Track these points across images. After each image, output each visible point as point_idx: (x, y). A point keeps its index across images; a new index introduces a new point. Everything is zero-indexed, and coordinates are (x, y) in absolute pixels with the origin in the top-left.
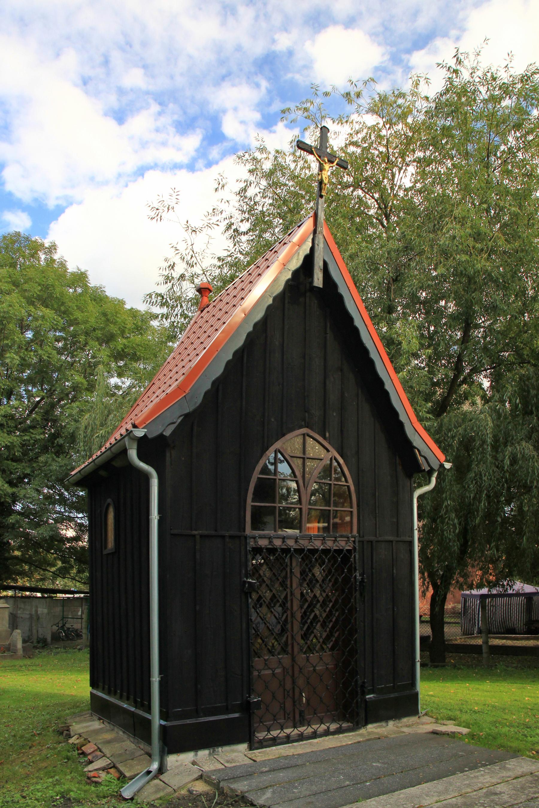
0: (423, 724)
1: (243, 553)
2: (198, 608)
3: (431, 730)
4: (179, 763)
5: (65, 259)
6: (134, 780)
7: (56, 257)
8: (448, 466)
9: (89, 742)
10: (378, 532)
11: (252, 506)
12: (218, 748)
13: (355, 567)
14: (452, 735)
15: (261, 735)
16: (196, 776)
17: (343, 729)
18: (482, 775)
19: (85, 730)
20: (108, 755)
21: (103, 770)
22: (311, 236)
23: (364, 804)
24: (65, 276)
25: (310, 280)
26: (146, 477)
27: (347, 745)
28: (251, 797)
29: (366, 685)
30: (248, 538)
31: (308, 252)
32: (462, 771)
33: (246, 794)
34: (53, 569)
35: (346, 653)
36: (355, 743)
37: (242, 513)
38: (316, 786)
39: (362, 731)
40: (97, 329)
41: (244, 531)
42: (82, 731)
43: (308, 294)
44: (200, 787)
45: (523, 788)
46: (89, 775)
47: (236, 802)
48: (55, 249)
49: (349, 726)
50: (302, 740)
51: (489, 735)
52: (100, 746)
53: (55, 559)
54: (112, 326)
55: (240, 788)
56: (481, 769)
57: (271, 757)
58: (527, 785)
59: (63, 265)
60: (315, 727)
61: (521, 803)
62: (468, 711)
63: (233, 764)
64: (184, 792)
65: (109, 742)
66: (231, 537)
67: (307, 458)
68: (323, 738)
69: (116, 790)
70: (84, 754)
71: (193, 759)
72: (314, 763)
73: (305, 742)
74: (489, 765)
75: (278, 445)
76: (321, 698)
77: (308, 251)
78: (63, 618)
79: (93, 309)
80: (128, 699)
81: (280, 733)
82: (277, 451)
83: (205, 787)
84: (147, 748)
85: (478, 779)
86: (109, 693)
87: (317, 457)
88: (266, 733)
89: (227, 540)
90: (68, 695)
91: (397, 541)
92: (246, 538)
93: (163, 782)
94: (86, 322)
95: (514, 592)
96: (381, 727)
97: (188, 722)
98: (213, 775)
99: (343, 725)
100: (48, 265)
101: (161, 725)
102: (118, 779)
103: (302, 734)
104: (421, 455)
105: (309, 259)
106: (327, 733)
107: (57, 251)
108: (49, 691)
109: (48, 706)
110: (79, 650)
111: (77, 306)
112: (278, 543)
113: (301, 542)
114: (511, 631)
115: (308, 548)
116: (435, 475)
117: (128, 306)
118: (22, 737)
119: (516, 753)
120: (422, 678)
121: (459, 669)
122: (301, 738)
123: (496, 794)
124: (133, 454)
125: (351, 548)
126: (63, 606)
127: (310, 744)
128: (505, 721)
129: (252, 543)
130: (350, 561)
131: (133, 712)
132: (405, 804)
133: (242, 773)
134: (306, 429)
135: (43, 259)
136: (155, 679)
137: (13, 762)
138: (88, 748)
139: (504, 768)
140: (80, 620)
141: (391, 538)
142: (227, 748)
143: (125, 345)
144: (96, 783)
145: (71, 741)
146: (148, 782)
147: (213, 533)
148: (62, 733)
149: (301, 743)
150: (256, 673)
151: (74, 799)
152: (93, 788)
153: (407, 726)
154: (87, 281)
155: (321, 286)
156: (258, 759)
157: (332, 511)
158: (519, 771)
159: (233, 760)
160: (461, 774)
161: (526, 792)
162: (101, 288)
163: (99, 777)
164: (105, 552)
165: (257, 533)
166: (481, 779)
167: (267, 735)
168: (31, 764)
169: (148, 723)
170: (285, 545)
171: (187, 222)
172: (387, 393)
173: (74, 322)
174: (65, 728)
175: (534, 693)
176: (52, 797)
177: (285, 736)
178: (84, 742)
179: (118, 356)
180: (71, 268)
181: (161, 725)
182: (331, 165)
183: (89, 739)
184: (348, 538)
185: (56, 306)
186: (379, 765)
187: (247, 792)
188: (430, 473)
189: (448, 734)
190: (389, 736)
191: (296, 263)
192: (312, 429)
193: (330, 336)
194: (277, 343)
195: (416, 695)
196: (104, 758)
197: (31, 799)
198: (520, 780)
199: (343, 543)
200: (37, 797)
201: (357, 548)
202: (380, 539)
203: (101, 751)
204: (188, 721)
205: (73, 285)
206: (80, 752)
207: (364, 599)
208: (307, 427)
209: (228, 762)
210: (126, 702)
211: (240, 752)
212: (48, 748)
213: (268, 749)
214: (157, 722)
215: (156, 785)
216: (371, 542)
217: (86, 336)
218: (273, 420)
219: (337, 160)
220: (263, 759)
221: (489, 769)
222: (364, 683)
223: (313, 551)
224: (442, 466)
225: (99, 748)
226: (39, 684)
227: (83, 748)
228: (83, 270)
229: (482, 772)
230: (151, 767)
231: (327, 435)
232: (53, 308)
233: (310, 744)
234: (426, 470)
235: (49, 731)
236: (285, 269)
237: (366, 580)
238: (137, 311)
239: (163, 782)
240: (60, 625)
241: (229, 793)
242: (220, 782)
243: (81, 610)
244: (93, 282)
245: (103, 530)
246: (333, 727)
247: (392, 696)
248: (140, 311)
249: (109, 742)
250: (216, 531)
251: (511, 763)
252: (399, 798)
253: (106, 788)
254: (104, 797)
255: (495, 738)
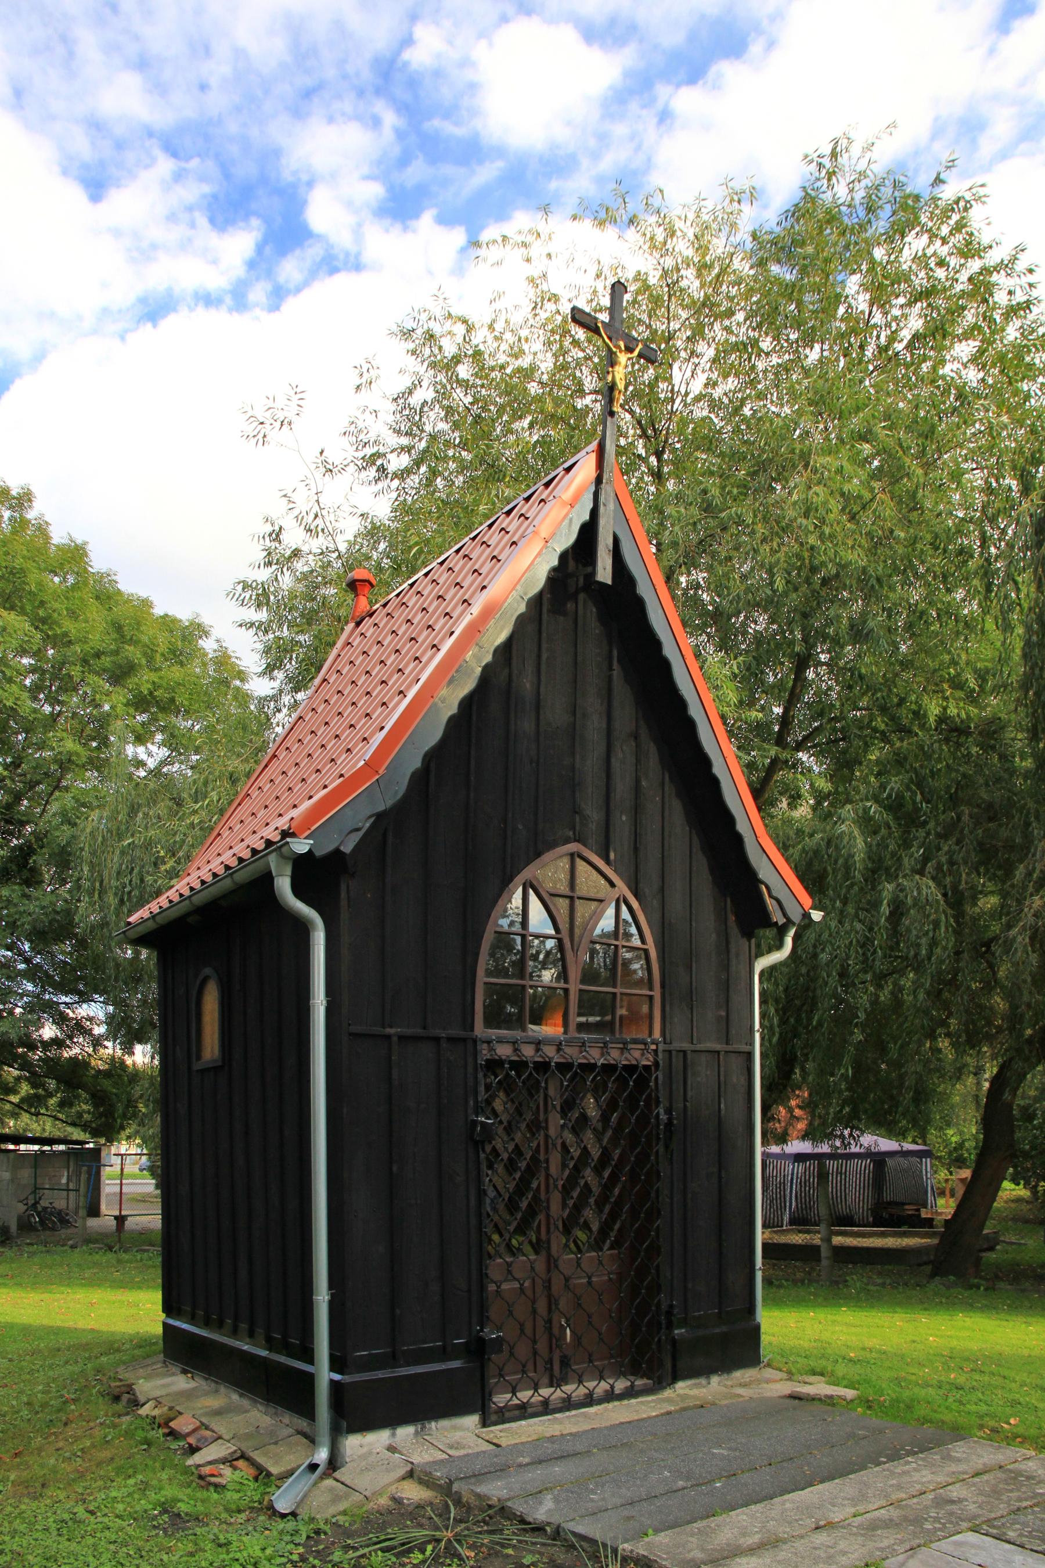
0: (768, 1381)
1: (470, 1069)
2: (395, 1168)
3: (788, 1392)
4: (365, 1450)
5: (46, 519)
6: (291, 1479)
7: (31, 515)
8: (817, 916)
9: (180, 1413)
10: (695, 1034)
11: (485, 983)
12: (430, 1423)
13: (658, 1098)
14: (829, 1401)
15: (501, 1399)
16: (402, 1471)
17: (636, 1388)
18: (915, 1470)
19: (163, 1392)
20: (227, 1437)
21: (224, 1463)
22: (593, 488)
23: (728, 1520)
24: (47, 549)
25: (589, 569)
26: (303, 928)
27: (649, 1418)
28: (519, 1507)
29: (676, 1311)
30: (479, 1043)
31: (588, 518)
32: (878, 1464)
33: (509, 1504)
34: (15, 1099)
35: (642, 1254)
36: (662, 1414)
37: (469, 997)
38: (628, 1489)
39: (668, 1393)
40: (103, 653)
41: (472, 1029)
42: (157, 1393)
43: (582, 596)
44: (413, 1493)
45: (996, 1493)
46: (203, 1473)
47: (491, 1517)
48: (30, 501)
49: (645, 1384)
50: (568, 1410)
51: (898, 1401)
52: (204, 1420)
53: (18, 1079)
54: (131, 648)
55: (494, 1492)
56: (909, 1459)
57: (524, 1439)
58: (1001, 1486)
59: (42, 530)
60: (591, 1384)
61: (1002, 1517)
62: (840, 1360)
63: (462, 1452)
64: (384, 1501)
65: (218, 1413)
66: (451, 1040)
67: (579, 898)
68: (603, 1406)
69: (256, 1498)
70: (173, 1434)
71: (387, 1442)
72: (605, 1448)
73: (574, 1412)
74: (922, 1452)
75: (526, 874)
76: (600, 1334)
77: (586, 517)
78: (36, 1188)
79: (96, 615)
80: (251, 1334)
81: (533, 1396)
82: (528, 885)
83: (422, 1492)
84: (303, 1424)
85: (911, 1476)
86: (207, 1324)
87: (592, 895)
88: (510, 1395)
89: (444, 1044)
90: (84, 1330)
91: (726, 1052)
92: (475, 1041)
93: (343, 1483)
94: (85, 641)
95: (862, 1150)
96: (696, 1386)
97: (381, 1376)
98: (436, 1470)
99: (637, 1383)
100: (15, 532)
101: (332, 1381)
102: (256, 1479)
103: (569, 1397)
104: (771, 896)
105: (588, 532)
106: (610, 1396)
107: (34, 504)
108: (46, 1322)
109: (59, 1350)
110: (72, 1247)
111: (67, 609)
112: (528, 1051)
113: (568, 1050)
114: (844, 1221)
115: (580, 1061)
116: (792, 932)
117: (158, 611)
118: (44, 1405)
119: (957, 1433)
120: (767, 1301)
121: (780, 1286)
122: (568, 1404)
123: (953, 1502)
124: (284, 885)
125: (649, 1063)
126: (36, 1167)
127: (585, 1415)
128: (913, 1378)
129: (485, 1053)
130: (649, 1086)
131: (265, 1358)
132: (801, 1519)
133: (486, 1466)
134: (576, 844)
135: (6, 518)
136: (322, 1297)
137: (40, 1450)
138: (183, 1424)
139: (948, 1457)
140: (65, 1193)
141: (718, 1047)
142: (444, 1423)
143: (154, 682)
144: (216, 1486)
145: (143, 1411)
146: (315, 1484)
147: (419, 1031)
148: (117, 1399)
149: (568, 1413)
150: (492, 1287)
151: (187, 1514)
152: (215, 1496)
153: (742, 1385)
154: (87, 563)
155: (609, 582)
156: (503, 1442)
157: (618, 996)
158: (979, 1463)
159: (458, 1443)
160: (877, 1469)
161: (1004, 1497)
162: (109, 575)
163: (221, 1475)
164: (197, 1066)
165: (494, 1033)
166: (916, 1476)
167: (511, 1399)
168: (79, 1453)
169: (309, 1381)
170: (541, 1056)
171: (322, 453)
172: (715, 782)
173: (62, 641)
174: (124, 1389)
175: (939, 1330)
176: (146, 1511)
177: (541, 1401)
178: (172, 1414)
179: (141, 703)
180: (58, 536)
181: (332, 1381)
182: (629, 355)
183: (178, 1408)
184: (645, 1044)
185: (28, 608)
186: (725, 1452)
187: (509, 1499)
188: (782, 931)
189: (820, 1399)
190: (717, 1402)
191: (567, 539)
192: (585, 845)
193: (617, 672)
194: (528, 686)
195: (757, 1328)
196: (220, 1441)
197: (105, 1515)
198: (985, 1477)
199: (637, 1054)
200: (117, 1512)
201: (661, 1062)
202: (699, 1047)
203: (207, 1428)
204: (381, 1374)
205: (62, 569)
206: (167, 1431)
207: (672, 1155)
208: (578, 841)
209: (451, 1447)
210: (248, 1340)
211: (468, 1429)
212: (101, 1424)
213: (513, 1425)
214: (324, 1375)
215: (331, 1490)
216: (684, 1052)
217: (83, 667)
218: (520, 827)
219: (640, 346)
220: (513, 1442)
221: (922, 1459)
222: (671, 1306)
223: (589, 1067)
224: (806, 916)
225: (202, 1424)
226: (23, 1311)
227: (172, 1424)
228: (79, 541)
229: (914, 1465)
230: (316, 1456)
231: (612, 856)
232: (23, 612)
233: (585, 1415)
234: (780, 923)
235: (91, 1395)
236: (547, 547)
237: (675, 1122)
238: (175, 621)
239: (343, 1483)
240: (31, 1202)
241: (472, 1500)
242: (451, 1482)
243: (66, 1174)
244: (98, 562)
245: (194, 1025)
246: (621, 1385)
247: (717, 1330)
248: (181, 621)
249: (218, 1413)
250: (425, 1028)
251: (959, 1449)
252: (786, 1510)
253: (236, 1496)
254: (239, 1511)
255: (909, 1407)
